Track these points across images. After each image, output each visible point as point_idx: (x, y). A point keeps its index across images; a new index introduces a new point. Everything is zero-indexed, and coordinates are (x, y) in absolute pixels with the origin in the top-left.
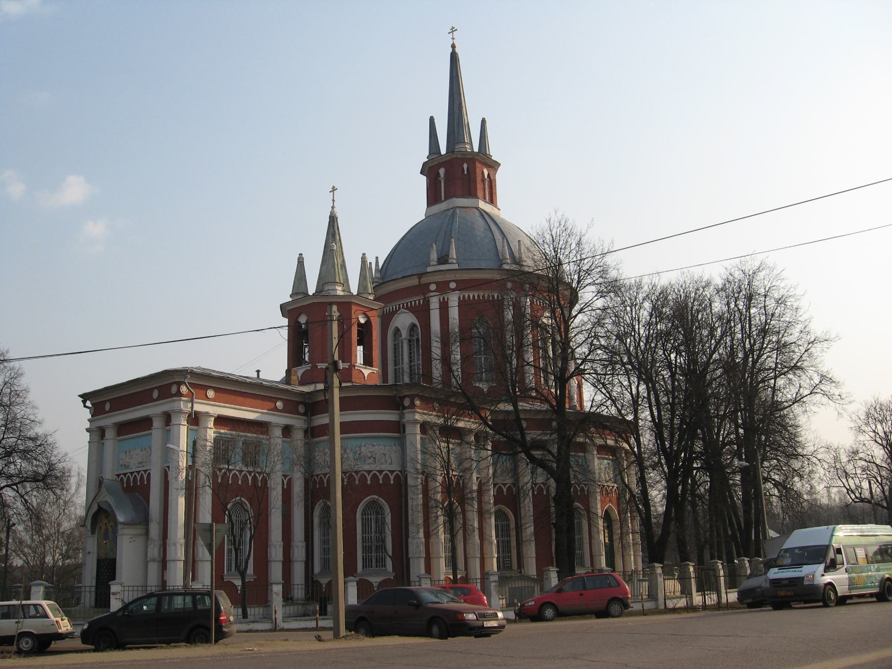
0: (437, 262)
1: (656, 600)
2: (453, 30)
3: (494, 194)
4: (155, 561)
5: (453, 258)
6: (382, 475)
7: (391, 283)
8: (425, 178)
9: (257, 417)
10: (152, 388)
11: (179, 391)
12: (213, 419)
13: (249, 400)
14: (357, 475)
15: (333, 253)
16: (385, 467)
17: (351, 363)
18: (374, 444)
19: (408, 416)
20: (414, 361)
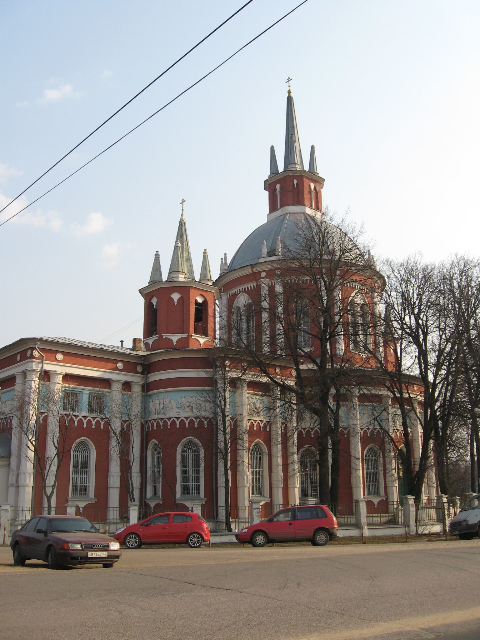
0: (267, 255)
1: (408, 526)
2: (289, 80)
3: (319, 203)
4: (13, 486)
6: (77, 419)
9: (98, 375)
11: (32, 354)
12: (61, 376)
13: (93, 362)
14: (169, 421)
17: (189, 334)
18: (192, 395)
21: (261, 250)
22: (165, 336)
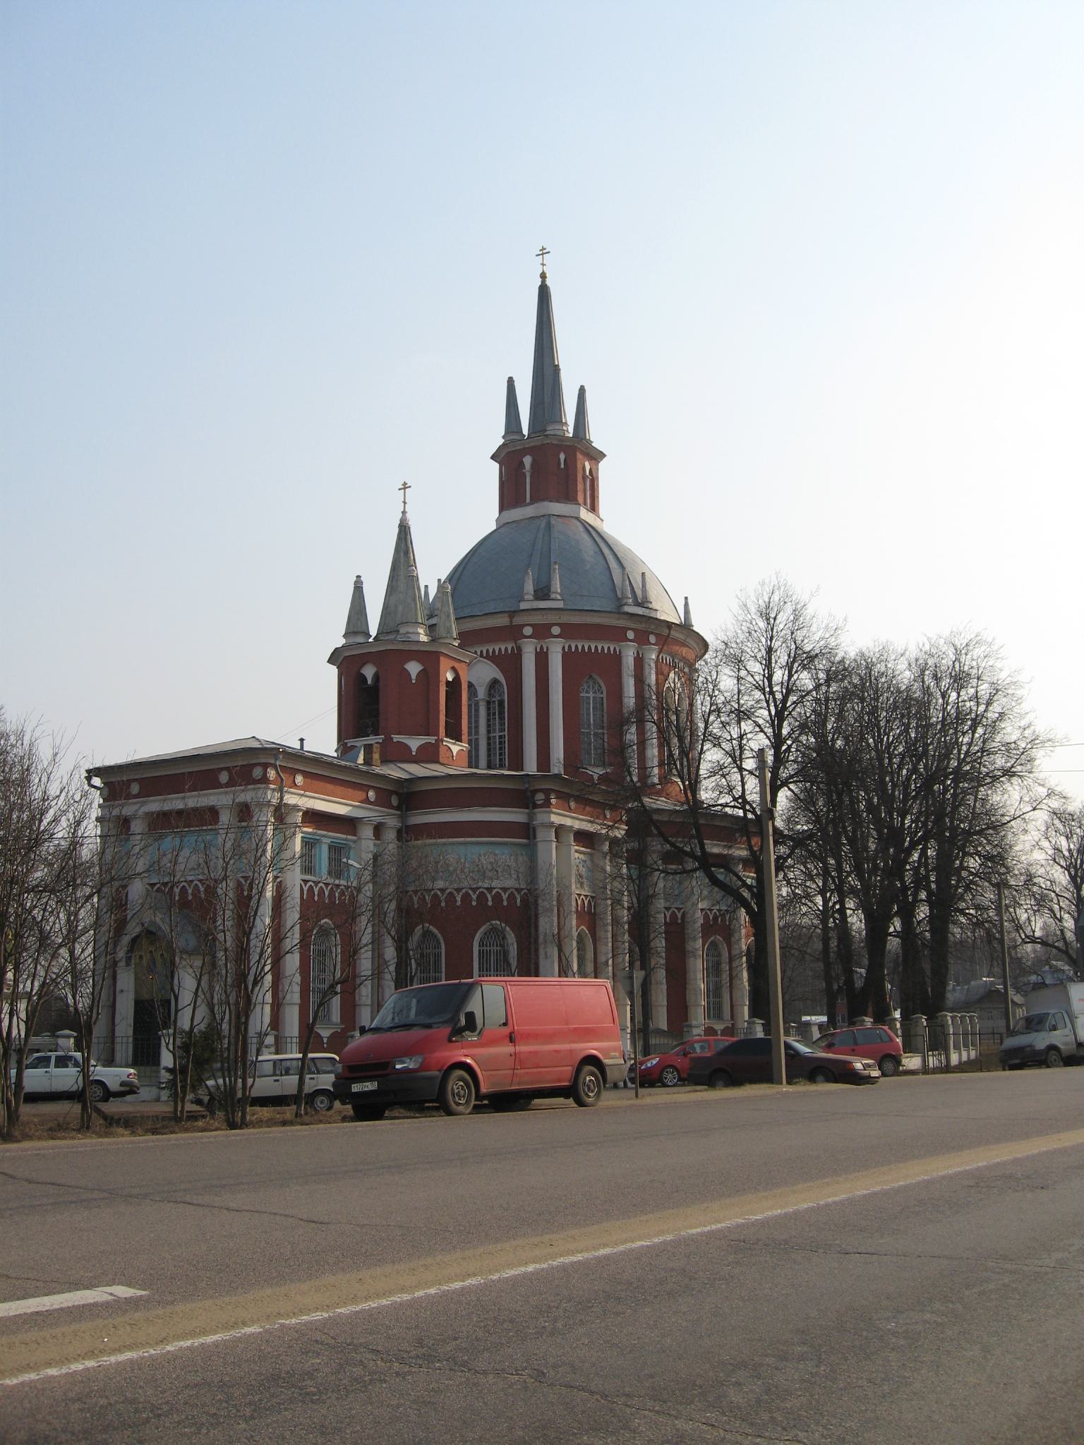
5: (557, 593)
6: (461, 894)
7: (467, 620)
8: (497, 465)
10: (218, 769)
12: (301, 814)
13: (339, 789)
14: (475, 893)
15: (413, 580)
16: (510, 883)
19: (541, 817)
20: (494, 731)
21: (522, 588)
22: (396, 738)
